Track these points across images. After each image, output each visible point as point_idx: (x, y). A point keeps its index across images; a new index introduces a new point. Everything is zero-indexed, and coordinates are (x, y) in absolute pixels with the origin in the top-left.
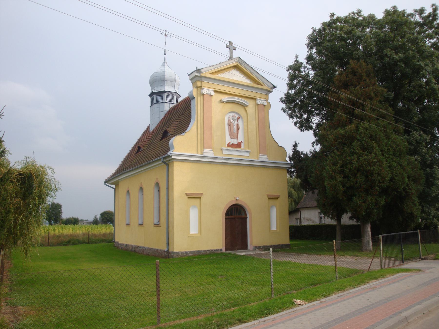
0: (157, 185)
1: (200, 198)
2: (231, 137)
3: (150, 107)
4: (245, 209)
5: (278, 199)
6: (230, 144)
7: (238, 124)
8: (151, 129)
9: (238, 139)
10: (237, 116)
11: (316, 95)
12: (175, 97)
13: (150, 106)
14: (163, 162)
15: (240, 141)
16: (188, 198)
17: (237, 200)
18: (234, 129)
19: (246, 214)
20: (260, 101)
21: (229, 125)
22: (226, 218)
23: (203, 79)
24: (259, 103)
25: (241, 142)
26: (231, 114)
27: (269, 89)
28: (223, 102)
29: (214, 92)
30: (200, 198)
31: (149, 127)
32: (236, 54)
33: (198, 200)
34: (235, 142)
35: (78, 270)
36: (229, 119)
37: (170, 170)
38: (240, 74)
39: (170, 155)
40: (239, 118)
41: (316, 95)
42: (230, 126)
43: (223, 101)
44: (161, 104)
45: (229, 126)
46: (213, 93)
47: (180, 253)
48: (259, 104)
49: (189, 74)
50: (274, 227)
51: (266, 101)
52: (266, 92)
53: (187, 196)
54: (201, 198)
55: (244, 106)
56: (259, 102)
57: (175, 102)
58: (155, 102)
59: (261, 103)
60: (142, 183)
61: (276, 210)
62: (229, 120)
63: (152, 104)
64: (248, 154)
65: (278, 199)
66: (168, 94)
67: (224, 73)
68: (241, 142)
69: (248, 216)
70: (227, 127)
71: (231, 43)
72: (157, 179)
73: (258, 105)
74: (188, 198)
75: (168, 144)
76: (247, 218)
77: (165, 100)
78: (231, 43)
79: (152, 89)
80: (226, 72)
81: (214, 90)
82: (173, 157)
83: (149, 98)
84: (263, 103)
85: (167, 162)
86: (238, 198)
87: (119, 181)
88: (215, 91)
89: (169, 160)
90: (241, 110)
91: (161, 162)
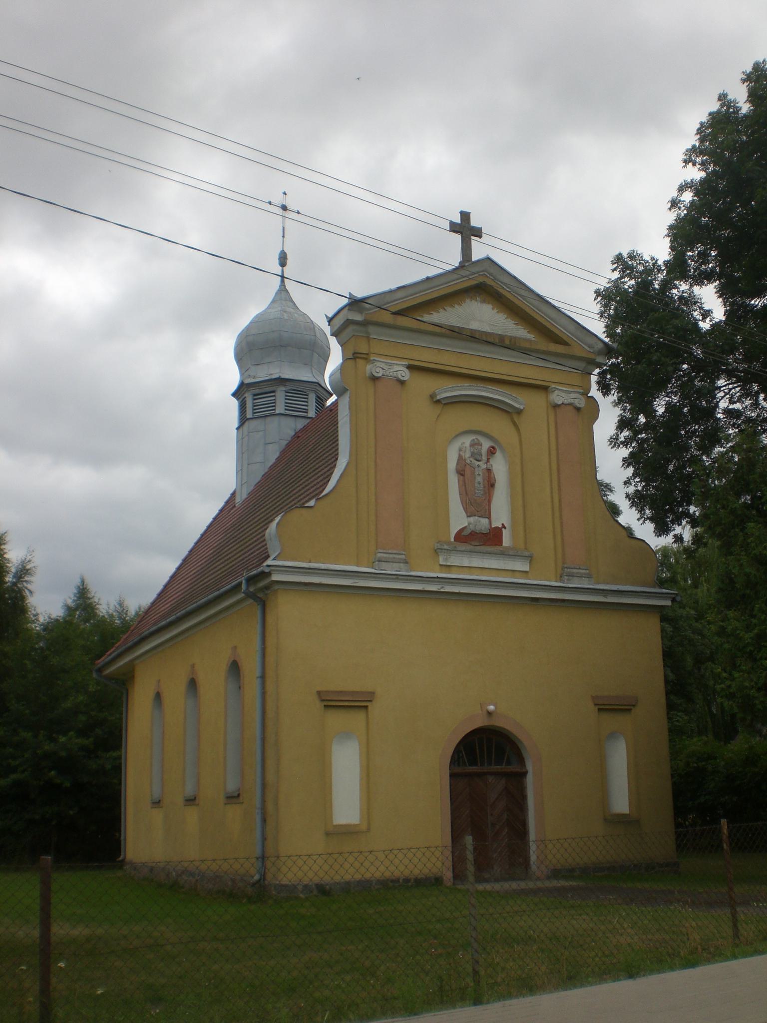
0: (235, 668)
1: (366, 707)
2: (466, 510)
3: (237, 429)
4: (520, 746)
5: (630, 710)
6: (466, 533)
7: (489, 471)
8: (238, 500)
9: (489, 518)
10: (486, 444)
11: (683, 346)
12: (312, 397)
13: (236, 425)
14: (250, 595)
15: (496, 524)
16: (325, 706)
17: (490, 714)
18: (477, 485)
19: (521, 761)
20: (563, 395)
21: (461, 472)
22: (452, 776)
23: (371, 329)
24: (560, 403)
25: (500, 526)
26: (467, 440)
27: (591, 356)
28: (438, 401)
29: (407, 371)
30: (366, 707)
31: (233, 494)
32: (479, 251)
33: (360, 716)
34: (482, 524)
35: (471, 953)
36: (459, 455)
37: (270, 619)
38: (496, 311)
39: (267, 570)
40: (492, 452)
41: (683, 346)
42: (462, 475)
43: (438, 398)
44: (269, 419)
45: (462, 477)
46: (405, 374)
47: (300, 887)
48: (559, 406)
49: (330, 315)
50: (621, 804)
51: (583, 394)
52: (582, 365)
53: (323, 701)
54: (370, 708)
55: (512, 413)
56: (558, 397)
57: (312, 413)
58: (249, 414)
59: (566, 402)
60: (193, 666)
61: (624, 746)
62: (460, 459)
63: (243, 419)
64: (521, 565)
65: (630, 710)
66: (289, 388)
67: (441, 310)
68: (500, 526)
69: (530, 766)
70: (453, 481)
71: (465, 216)
72: (235, 648)
73: (556, 406)
74: (325, 706)
75: (264, 538)
76: (524, 774)
77: (280, 409)
78: (465, 216)
79: (242, 374)
80: (448, 309)
81: (406, 363)
82: (275, 577)
83: (235, 403)
84: (572, 401)
85: (260, 595)
86: (491, 708)
87: (137, 662)
88: (410, 367)
89: (267, 588)
90: (498, 426)
91: (241, 596)
